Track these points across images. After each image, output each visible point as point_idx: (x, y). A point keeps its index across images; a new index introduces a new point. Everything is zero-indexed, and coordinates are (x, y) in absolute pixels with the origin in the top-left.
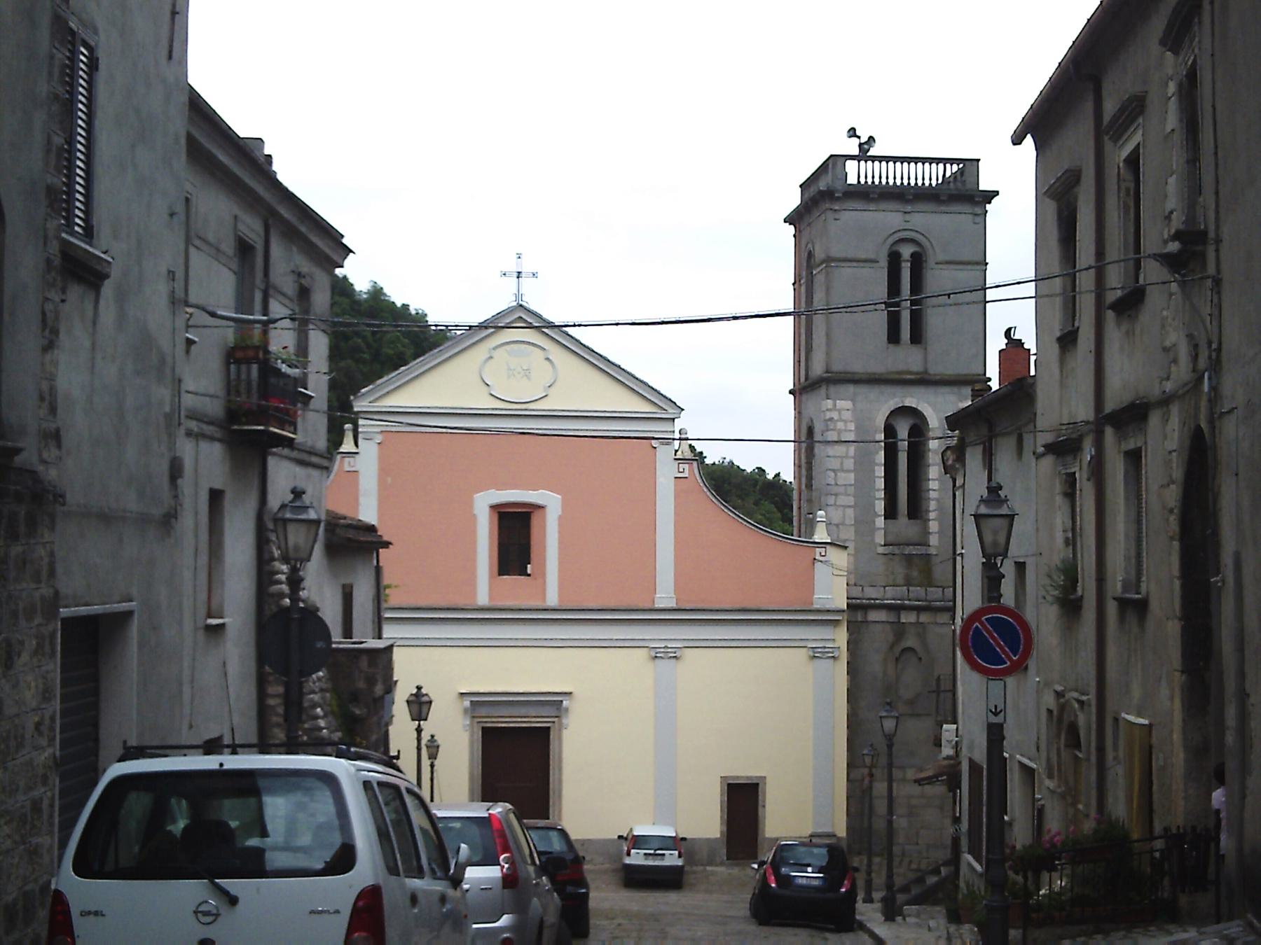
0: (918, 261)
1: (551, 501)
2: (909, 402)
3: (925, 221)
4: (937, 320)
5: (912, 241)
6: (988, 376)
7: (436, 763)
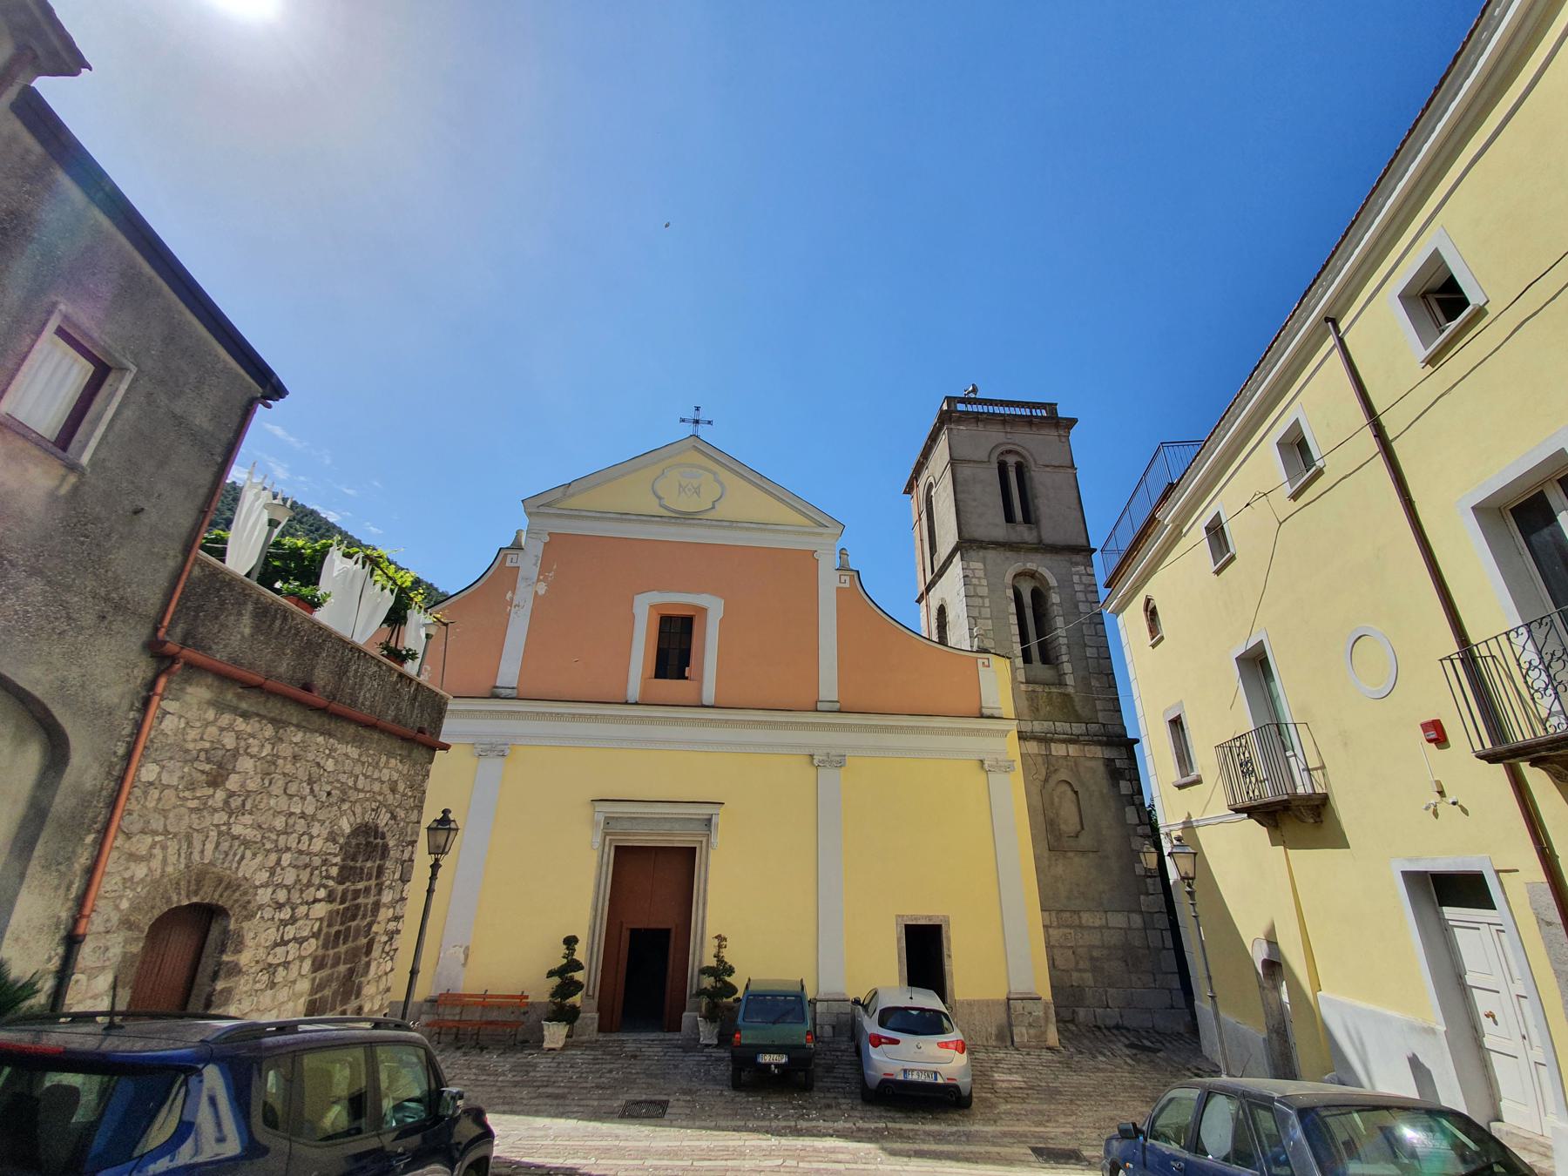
0: (1020, 468)
1: (714, 607)
2: (1031, 566)
3: (1027, 440)
4: (1046, 506)
5: (1017, 453)
6: (1092, 547)
7: (445, 861)
